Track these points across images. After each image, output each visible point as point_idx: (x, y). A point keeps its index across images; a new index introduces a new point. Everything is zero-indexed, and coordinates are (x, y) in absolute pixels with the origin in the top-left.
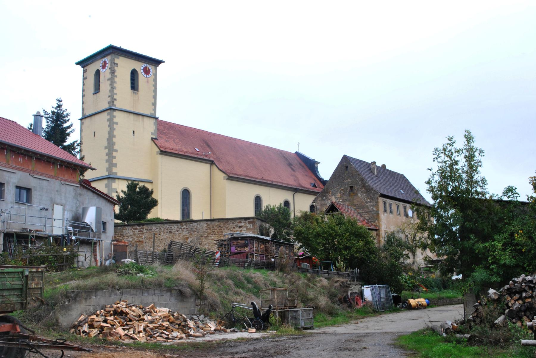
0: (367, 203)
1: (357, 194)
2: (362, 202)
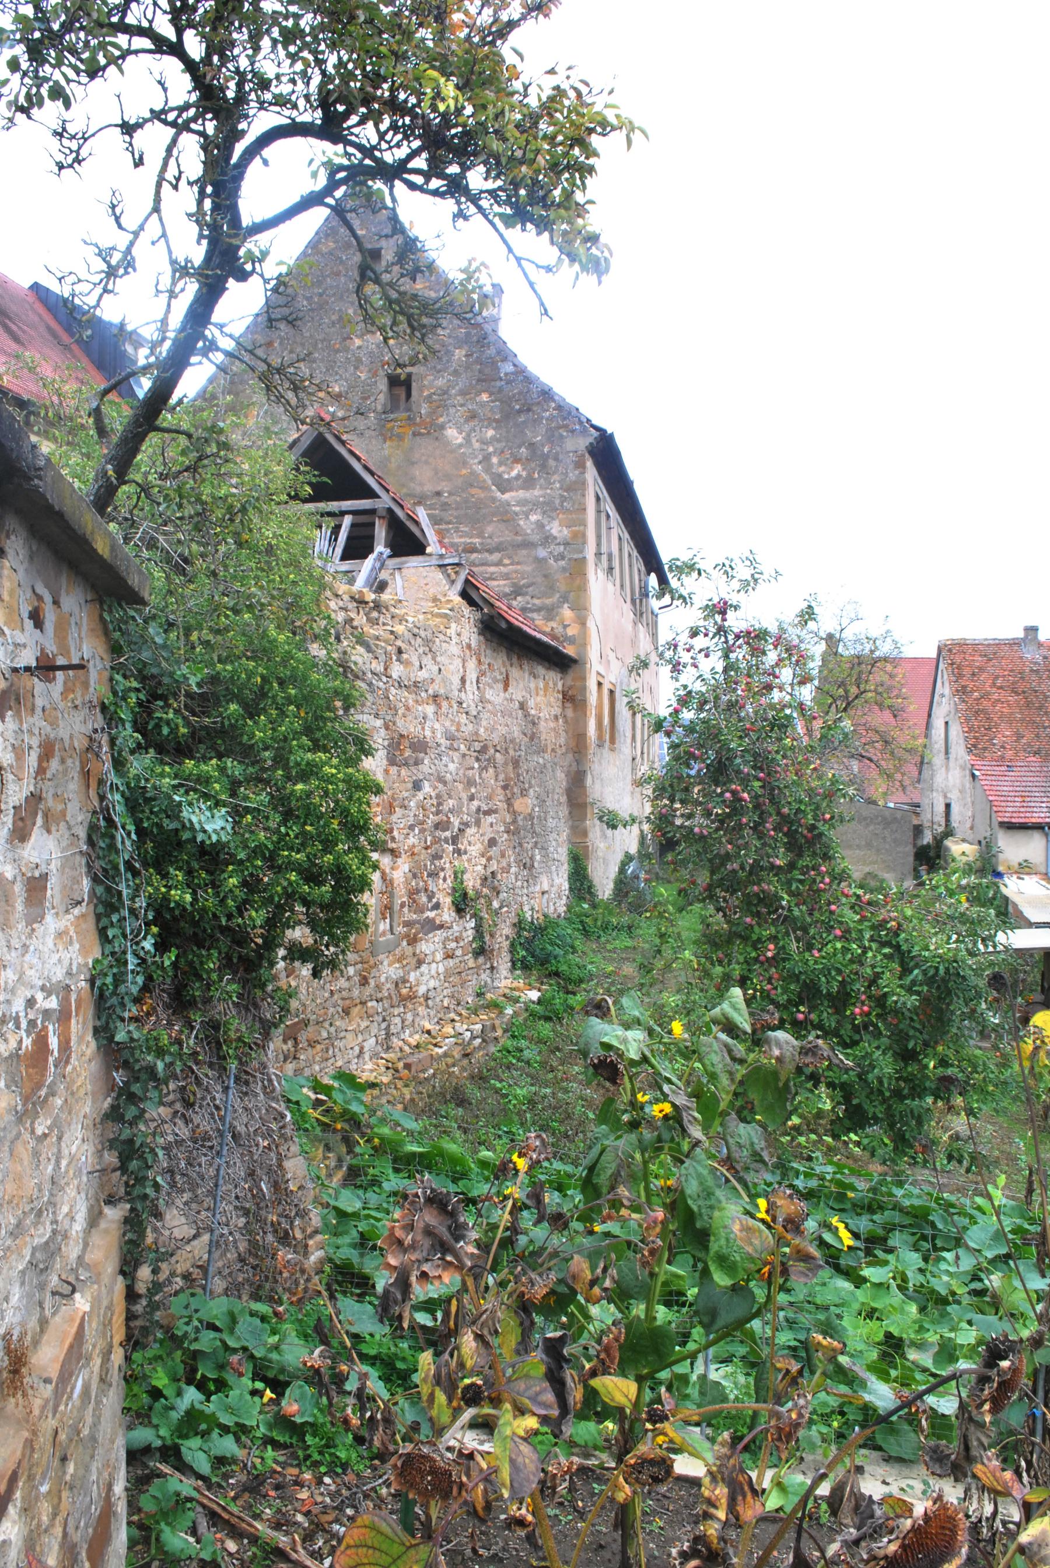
0: (504, 486)
1: (434, 430)
2: (472, 481)
